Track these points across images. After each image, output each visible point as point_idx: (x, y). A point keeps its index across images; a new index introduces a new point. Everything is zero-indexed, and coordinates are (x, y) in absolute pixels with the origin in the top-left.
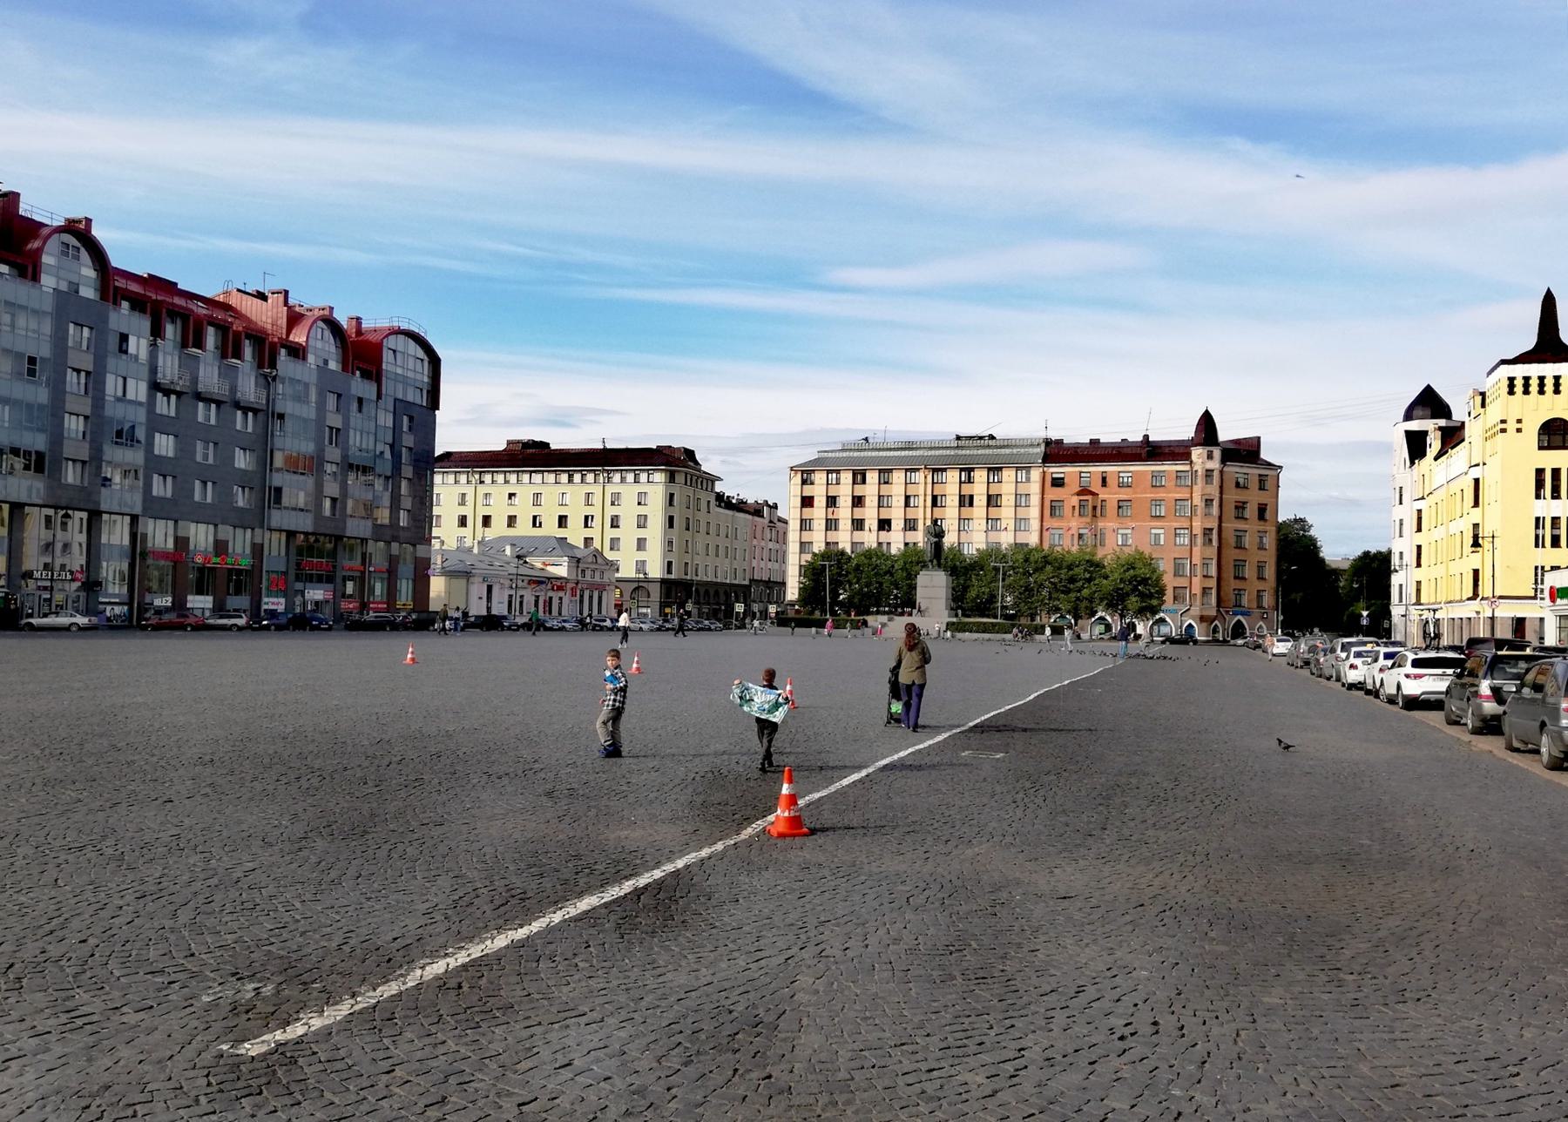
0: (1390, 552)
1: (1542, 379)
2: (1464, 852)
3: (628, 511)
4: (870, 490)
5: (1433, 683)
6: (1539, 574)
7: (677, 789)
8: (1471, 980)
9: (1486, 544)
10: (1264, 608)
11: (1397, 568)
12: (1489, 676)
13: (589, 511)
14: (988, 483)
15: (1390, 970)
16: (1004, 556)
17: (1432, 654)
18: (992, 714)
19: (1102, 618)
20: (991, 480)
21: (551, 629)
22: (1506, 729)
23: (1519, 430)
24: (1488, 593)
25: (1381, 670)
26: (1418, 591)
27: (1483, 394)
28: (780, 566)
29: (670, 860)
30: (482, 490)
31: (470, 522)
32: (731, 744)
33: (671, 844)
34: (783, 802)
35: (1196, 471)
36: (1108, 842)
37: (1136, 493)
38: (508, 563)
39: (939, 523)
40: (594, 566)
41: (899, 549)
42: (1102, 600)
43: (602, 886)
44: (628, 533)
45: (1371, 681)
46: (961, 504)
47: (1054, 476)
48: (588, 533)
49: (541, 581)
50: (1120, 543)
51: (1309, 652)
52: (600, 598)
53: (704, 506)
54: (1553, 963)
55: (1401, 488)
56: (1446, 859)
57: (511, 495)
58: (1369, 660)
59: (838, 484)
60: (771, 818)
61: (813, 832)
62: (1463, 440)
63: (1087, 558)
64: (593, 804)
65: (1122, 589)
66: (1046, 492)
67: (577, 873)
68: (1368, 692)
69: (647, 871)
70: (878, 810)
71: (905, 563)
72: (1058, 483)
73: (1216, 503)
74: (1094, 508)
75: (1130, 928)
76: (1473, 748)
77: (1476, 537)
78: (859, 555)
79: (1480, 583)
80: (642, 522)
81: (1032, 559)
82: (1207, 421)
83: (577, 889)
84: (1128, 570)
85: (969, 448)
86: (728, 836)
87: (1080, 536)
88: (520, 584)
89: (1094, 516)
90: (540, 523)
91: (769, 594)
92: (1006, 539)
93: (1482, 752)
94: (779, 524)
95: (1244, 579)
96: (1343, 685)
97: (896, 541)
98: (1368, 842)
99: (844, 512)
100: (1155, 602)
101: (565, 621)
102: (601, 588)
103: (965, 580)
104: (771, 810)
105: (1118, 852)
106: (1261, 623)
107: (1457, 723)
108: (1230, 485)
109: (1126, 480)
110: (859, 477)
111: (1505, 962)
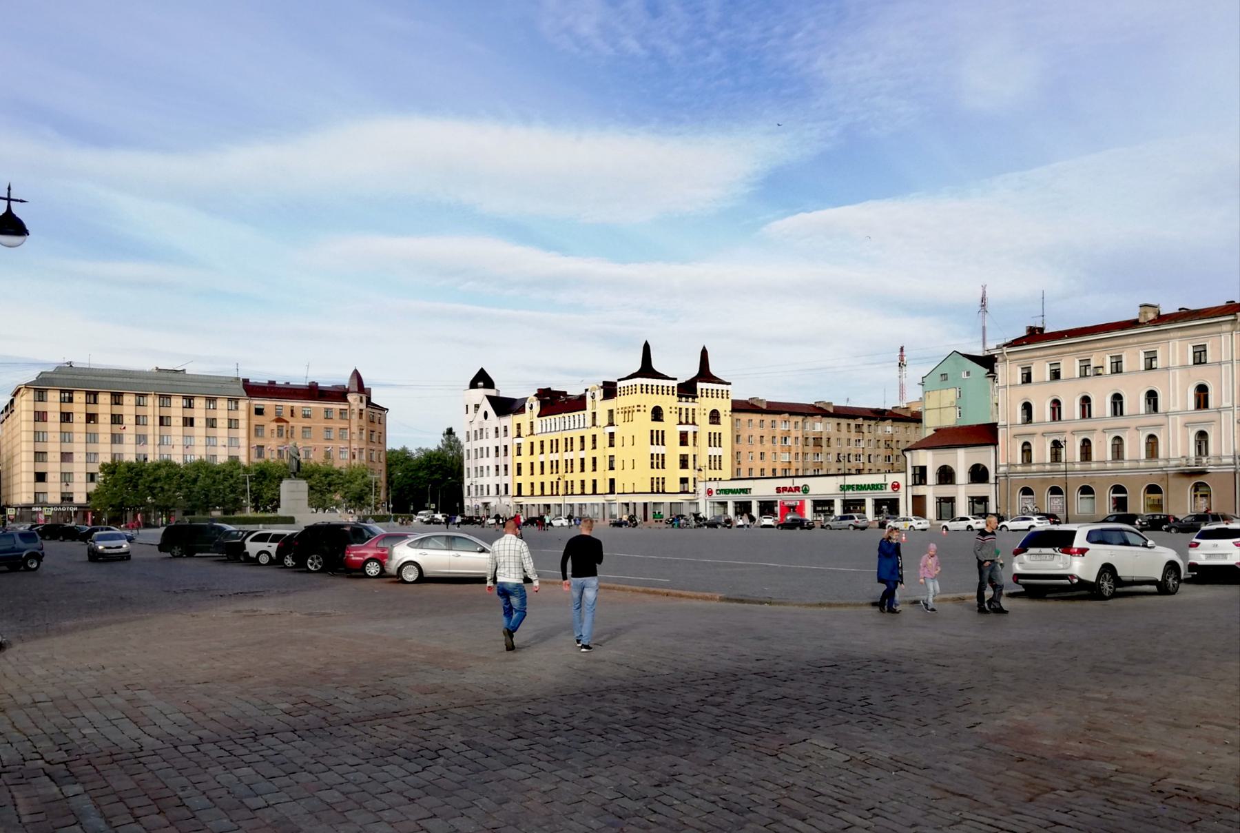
37: (315, 422)
52: (552, 489)
72: (259, 412)
82: (919, 384)
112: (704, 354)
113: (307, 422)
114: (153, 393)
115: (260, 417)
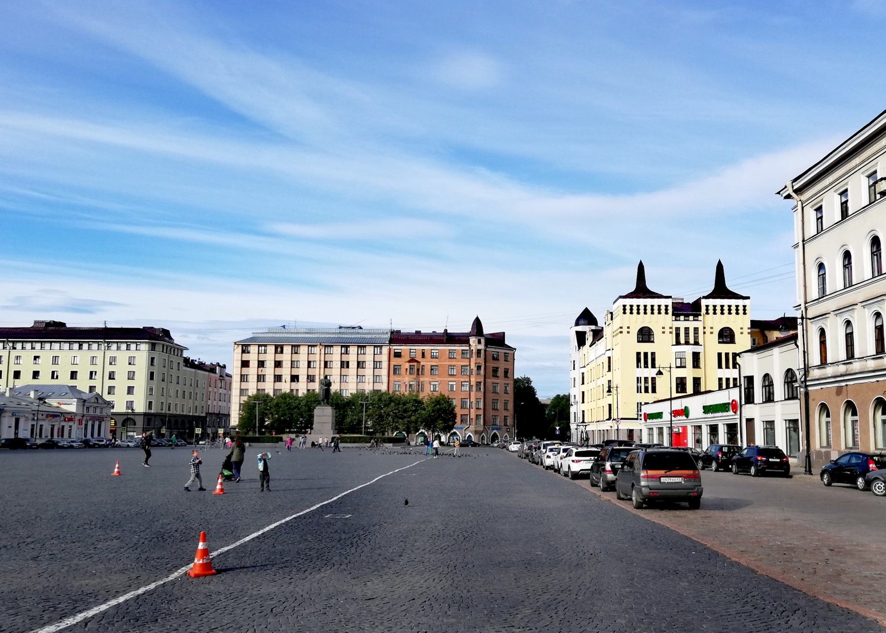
0: (569, 395)
1: (715, 306)
2: (587, 555)
3: (122, 370)
4: (286, 357)
5: (585, 464)
6: (639, 407)
7: (131, 550)
8: (579, 626)
9: (614, 391)
10: (508, 426)
11: (573, 404)
12: (610, 460)
13: (93, 368)
14: (358, 354)
15: (539, 625)
16: (367, 397)
17: (585, 449)
18: (349, 491)
19: (422, 433)
20: (359, 353)
21: (62, 447)
22: (617, 488)
23: (628, 332)
24: (615, 417)
25: (561, 458)
26: (583, 416)
27: (611, 313)
28: (227, 403)
29: (115, 597)
30: (14, 353)
31: (11, 375)
32: (174, 519)
33: (118, 586)
34: (199, 554)
35: (472, 350)
36: (401, 563)
38: (32, 403)
39: (328, 378)
40: (95, 405)
41: (303, 394)
42: (422, 422)
43: (60, 618)
44: (121, 383)
45: (557, 466)
46: (342, 367)
47: (396, 351)
48: (92, 383)
49: (55, 415)
50: (432, 390)
51: (529, 450)
53: (175, 366)
54: (621, 613)
55: (574, 361)
56: (578, 560)
57: (36, 358)
58: (556, 453)
59: (265, 353)
60: (191, 565)
61: (219, 572)
62: (603, 337)
63: (414, 398)
64: (67, 563)
65: (433, 416)
66: (391, 360)
67: (44, 611)
68: (556, 471)
69: (96, 606)
70: (265, 555)
71: (307, 402)
72: (398, 355)
73: (482, 368)
74: (418, 370)
75: (404, 613)
76: (601, 499)
77: (609, 387)
78: (278, 397)
79: (612, 411)
80: (131, 376)
81: (383, 399)
82: (477, 324)
83: (42, 622)
84: (436, 405)
85: (347, 333)
86: (161, 579)
87: (410, 385)
88: (40, 417)
89: (418, 374)
90: (57, 377)
91: (219, 422)
92: (368, 388)
93: (606, 500)
94: (227, 378)
95: (497, 410)
96: (544, 467)
97: (302, 388)
98: (541, 553)
99: (269, 370)
100: (451, 423)
101: (72, 442)
102: (101, 419)
103: (344, 412)
104: (192, 560)
105: (406, 569)
106: (506, 434)
107: (596, 486)
108: (490, 358)
109: (435, 354)
110: (279, 349)
111: (598, 614)
112: (720, 268)
113: (434, 362)
114: (319, 344)
115: (398, 359)
